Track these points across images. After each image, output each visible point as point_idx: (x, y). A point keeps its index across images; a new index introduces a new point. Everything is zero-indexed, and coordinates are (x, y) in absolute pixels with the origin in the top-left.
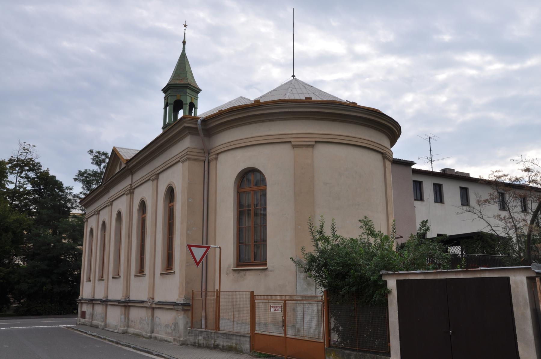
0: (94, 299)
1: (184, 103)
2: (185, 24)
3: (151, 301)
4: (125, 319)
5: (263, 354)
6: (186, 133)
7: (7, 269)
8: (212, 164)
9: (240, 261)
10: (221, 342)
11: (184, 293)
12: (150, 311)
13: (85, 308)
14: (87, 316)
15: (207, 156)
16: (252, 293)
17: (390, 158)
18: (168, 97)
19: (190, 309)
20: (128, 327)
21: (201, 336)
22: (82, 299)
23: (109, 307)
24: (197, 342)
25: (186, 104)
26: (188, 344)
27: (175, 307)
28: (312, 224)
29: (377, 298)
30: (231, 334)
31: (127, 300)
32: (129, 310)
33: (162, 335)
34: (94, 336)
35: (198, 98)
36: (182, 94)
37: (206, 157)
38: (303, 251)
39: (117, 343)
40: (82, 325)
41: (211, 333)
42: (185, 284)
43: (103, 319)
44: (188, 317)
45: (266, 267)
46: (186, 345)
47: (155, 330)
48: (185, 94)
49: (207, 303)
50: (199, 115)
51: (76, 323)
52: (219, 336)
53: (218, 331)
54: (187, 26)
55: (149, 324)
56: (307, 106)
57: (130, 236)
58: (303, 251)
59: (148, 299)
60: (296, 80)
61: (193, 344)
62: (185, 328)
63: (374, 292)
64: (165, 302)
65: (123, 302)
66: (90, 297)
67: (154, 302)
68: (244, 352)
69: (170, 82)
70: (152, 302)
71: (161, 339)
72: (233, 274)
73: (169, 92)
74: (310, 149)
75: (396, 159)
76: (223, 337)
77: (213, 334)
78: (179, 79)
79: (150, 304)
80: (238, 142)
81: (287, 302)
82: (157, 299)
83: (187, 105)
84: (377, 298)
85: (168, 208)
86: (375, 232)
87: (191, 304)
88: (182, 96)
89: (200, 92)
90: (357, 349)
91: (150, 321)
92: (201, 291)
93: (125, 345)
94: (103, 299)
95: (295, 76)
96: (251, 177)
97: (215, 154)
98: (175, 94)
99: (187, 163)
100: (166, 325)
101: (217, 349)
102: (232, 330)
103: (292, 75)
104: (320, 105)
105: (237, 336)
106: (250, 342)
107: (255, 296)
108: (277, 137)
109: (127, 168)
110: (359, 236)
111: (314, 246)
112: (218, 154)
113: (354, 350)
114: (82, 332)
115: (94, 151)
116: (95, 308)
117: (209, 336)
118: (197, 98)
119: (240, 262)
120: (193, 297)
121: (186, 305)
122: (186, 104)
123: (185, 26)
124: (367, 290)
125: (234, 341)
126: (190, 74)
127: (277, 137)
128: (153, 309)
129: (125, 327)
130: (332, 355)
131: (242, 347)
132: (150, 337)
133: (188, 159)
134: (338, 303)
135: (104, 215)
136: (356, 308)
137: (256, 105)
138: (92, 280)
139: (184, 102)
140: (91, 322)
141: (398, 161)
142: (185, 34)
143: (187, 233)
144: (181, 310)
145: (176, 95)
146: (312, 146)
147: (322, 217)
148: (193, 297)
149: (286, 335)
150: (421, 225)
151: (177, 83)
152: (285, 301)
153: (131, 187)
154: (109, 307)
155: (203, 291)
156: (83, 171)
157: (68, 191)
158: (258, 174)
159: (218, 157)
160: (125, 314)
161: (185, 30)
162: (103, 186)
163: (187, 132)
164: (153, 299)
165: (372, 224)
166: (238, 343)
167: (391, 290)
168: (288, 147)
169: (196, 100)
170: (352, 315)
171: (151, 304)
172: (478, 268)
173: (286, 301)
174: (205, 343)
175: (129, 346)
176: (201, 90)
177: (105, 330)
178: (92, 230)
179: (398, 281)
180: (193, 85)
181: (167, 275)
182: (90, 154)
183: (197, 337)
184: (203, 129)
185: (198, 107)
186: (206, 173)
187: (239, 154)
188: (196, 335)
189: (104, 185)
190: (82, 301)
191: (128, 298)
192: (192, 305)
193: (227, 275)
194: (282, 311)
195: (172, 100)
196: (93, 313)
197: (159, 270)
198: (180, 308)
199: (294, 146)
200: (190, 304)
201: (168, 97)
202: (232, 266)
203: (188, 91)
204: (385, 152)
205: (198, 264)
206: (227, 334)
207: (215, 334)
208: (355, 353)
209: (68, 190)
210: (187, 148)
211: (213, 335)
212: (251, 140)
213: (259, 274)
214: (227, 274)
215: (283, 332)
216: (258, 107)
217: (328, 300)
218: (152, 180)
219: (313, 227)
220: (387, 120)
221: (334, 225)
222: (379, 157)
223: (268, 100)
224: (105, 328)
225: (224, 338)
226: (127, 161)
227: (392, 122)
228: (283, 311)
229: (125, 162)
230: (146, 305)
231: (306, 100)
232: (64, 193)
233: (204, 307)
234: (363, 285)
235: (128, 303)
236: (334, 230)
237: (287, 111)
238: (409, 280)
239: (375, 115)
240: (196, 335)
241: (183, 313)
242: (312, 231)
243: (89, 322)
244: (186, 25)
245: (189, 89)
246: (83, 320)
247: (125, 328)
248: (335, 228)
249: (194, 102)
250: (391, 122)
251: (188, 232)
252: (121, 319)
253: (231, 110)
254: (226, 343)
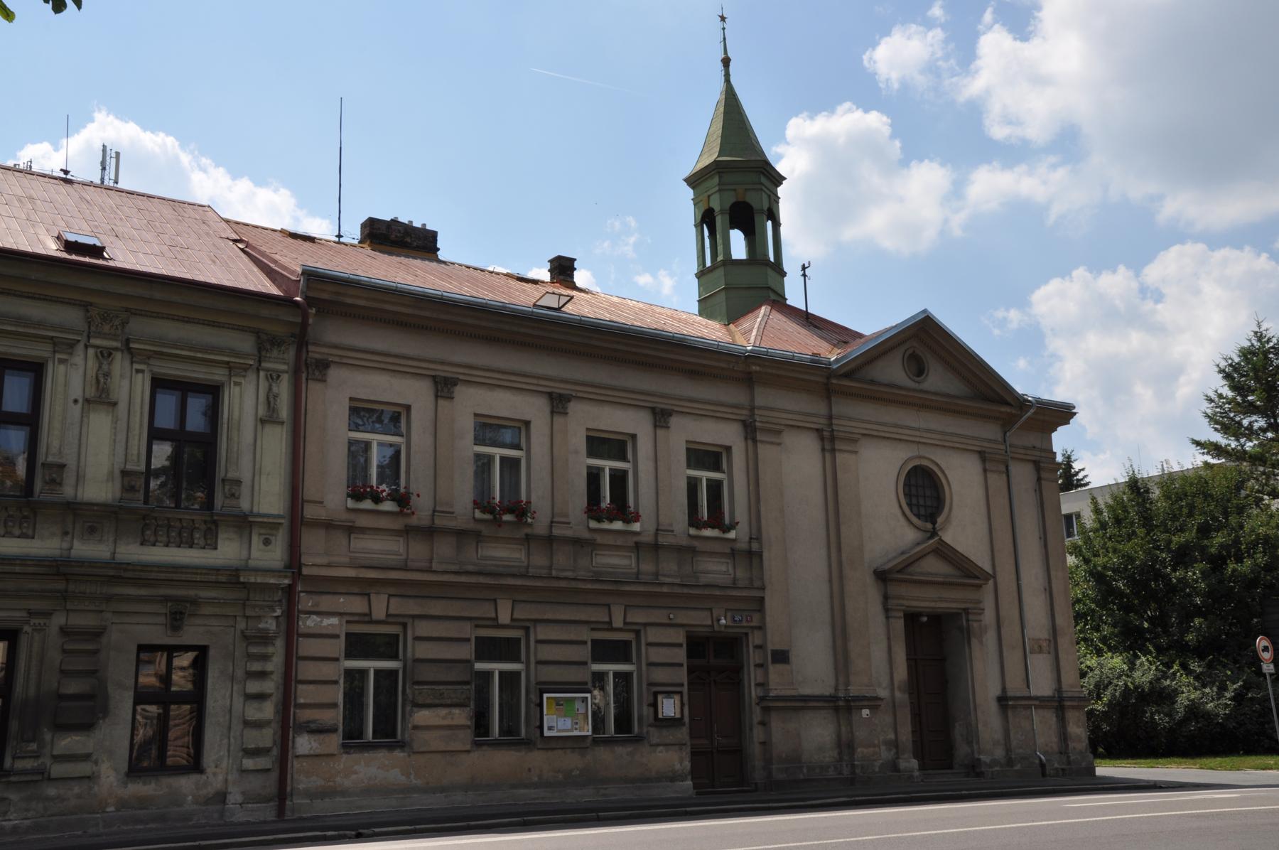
2: (721, 15)
7: (535, 789)
95: (342, 236)
103: (337, 234)
116: (1054, 686)
244: (725, 16)
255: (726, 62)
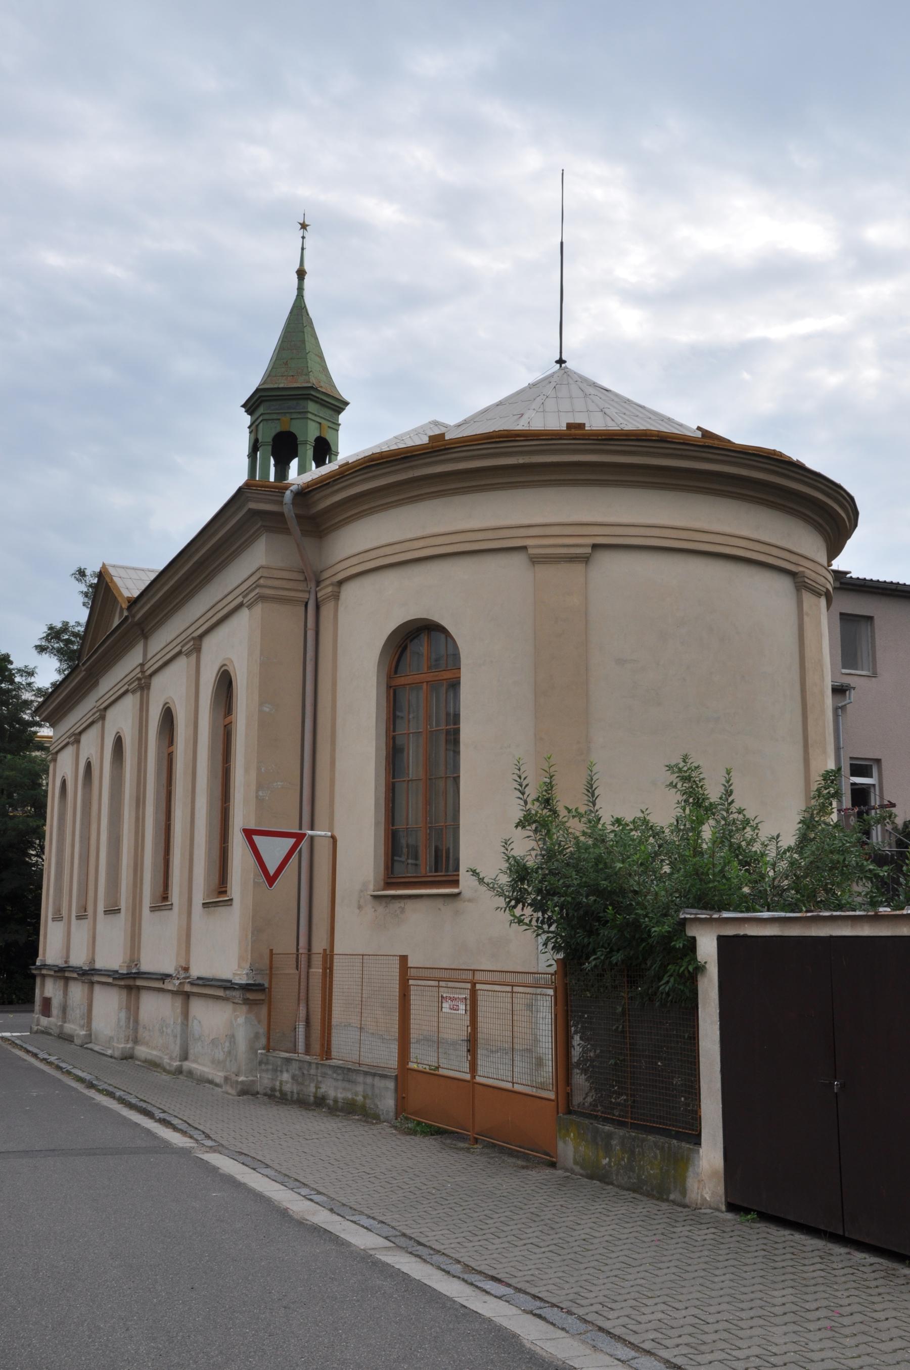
0: (69, 967)
1: (302, 439)
2: (302, 222)
3: (182, 975)
4: (129, 1021)
5: (673, 1133)
6: (256, 528)
8: (327, 611)
9: (392, 873)
10: (333, 1089)
11: (249, 957)
12: (179, 1002)
13: (50, 989)
14: (55, 1010)
15: (313, 590)
16: (404, 959)
17: (819, 587)
18: (257, 426)
19: (263, 1000)
20: (136, 1041)
21: (287, 1071)
22: (44, 966)
23: (97, 989)
24: (278, 1088)
25: (305, 443)
26: (258, 1093)
27: (229, 993)
28: (525, 779)
29: (670, 984)
30: (353, 1068)
31: (134, 971)
32: (138, 999)
33: (201, 1066)
34: (50, 1063)
35: (339, 425)
36: (294, 416)
37: (309, 592)
38: (507, 850)
39: (91, 1086)
40: (42, 1032)
41: (310, 1063)
42: (253, 933)
43: (83, 1019)
44: (259, 1022)
45: (456, 891)
46: (252, 1095)
47: (191, 1057)
48: (304, 415)
49: (310, 984)
50: (292, 480)
51: (31, 1028)
52: (327, 1074)
53: (327, 1059)
54: (308, 225)
55: (176, 1036)
56: (570, 447)
57: (140, 801)
58: (507, 850)
59: (176, 970)
60: (567, 372)
61: (269, 1092)
62: (252, 1050)
63: (664, 968)
64: (212, 980)
65: (123, 977)
66: (60, 963)
67: (188, 978)
68: (382, 1117)
69: (263, 384)
70: (185, 978)
71: (200, 1076)
72: (373, 907)
73: (261, 410)
74: (579, 568)
75: (892, 583)
76: (335, 1075)
77: (314, 1066)
78: (286, 374)
79: (177, 982)
80: (388, 550)
81: (478, 986)
82: (195, 972)
83: (308, 447)
84: (670, 984)
85: (222, 728)
86: (708, 799)
87: (267, 985)
88: (294, 422)
89: (343, 409)
90: (630, 1120)
91: (179, 1028)
92: (295, 951)
93: (106, 1090)
94: (120, 972)
95: (565, 362)
96: (422, 646)
97: (332, 584)
98: (275, 416)
99: (258, 608)
100: (213, 1041)
101: (323, 1108)
102: (358, 1059)
103: (558, 358)
104: (603, 444)
105: (366, 1073)
106: (396, 1090)
107: (410, 968)
108: (490, 535)
109: (130, 621)
110: (643, 812)
111: (528, 837)
112: (340, 583)
113: (621, 1124)
114: (28, 1052)
115: (88, 572)
117: (305, 1072)
118: (335, 426)
119: (392, 876)
120: (271, 968)
121: (254, 988)
122: (305, 443)
123: (304, 226)
124: (649, 963)
125: (360, 1089)
126: (318, 359)
127: (490, 535)
128: (187, 996)
129: (127, 1041)
130: (572, 1134)
131: (379, 1103)
132: (179, 1071)
133: (259, 597)
134: (589, 995)
135: (89, 745)
136: (629, 1009)
137: (432, 447)
138: (63, 915)
139: (300, 438)
140: (61, 1026)
141: (896, 590)
142: (303, 249)
143: (257, 797)
144: (241, 1002)
145: (279, 419)
146: (585, 559)
147: (549, 758)
148: (271, 968)
149: (473, 1077)
150: (823, 782)
151: (281, 386)
152: (474, 985)
153: (143, 672)
154: (97, 989)
155: (301, 951)
156: (59, 625)
157: (24, 678)
158: (443, 636)
159: (339, 592)
160: (128, 1009)
161: (303, 238)
162: (83, 669)
163: (259, 524)
164: (186, 969)
165: (702, 776)
166: (370, 1093)
167: (706, 963)
168: (518, 561)
169: (333, 431)
170: (618, 1027)
171: (180, 983)
172: (903, 909)
173: (475, 984)
174: (295, 1091)
175: (111, 1095)
176: (347, 404)
177: (87, 1048)
178: (64, 783)
179: (720, 939)
180: (324, 390)
181: (216, 908)
182: (77, 580)
183: (279, 1073)
184: (298, 516)
185: (339, 451)
186: (311, 634)
187: (390, 582)
188: (275, 1070)
189: (83, 664)
190: (44, 972)
191: (136, 965)
192: (270, 988)
193: (358, 911)
194: (466, 1010)
195: (268, 433)
196: (66, 1002)
197: (199, 898)
198: (237, 994)
199: (535, 560)
200: (264, 985)
201: (257, 426)
202: (371, 887)
203: (312, 407)
204: (801, 569)
205: (271, 880)
206: (344, 1068)
207: (317, 1068)
208: (621, 1132)
209: (22, 676)
210: (259, 569)
211: (313, 1071)
212: (421, 543)
213: (439, 909)
214: (360, 907)
215: (466, 1066)
216: (436, 454)
217: (566, 984)
218: (186, 655)
219: (527, 785)
220: (806, 480)
221: (595, 779)
222: (784, 585)
223: (474, 433)
224: (87, 1043)
225: (336, 1080)
226: (129, 602)
227: (819, 485)
228: (468, 1013)
229: (125, 605)
230: (170, 987)
231: (569, 432)
232: (11, 684)
233: (303, 995)
234: (641, 948)
235: (135, 978)
236: (593, 795)
237: (516, 462)
238: (745, 937)
239: (766, 466)
240: (275, 1070)
241: (244, 1008)
242: (526, 796)
243: (56, 1025)
244: (307, 223)
245: (312, 400)
246: (44, 1021)
247: (129, 1046)
248: (596, 789)
249: (328, 438)
250: (819, 485)
251: (260, 793)
252: (119, 1020)
253: (368, 464)
254: (341, 1093)
255: (301, 274)
